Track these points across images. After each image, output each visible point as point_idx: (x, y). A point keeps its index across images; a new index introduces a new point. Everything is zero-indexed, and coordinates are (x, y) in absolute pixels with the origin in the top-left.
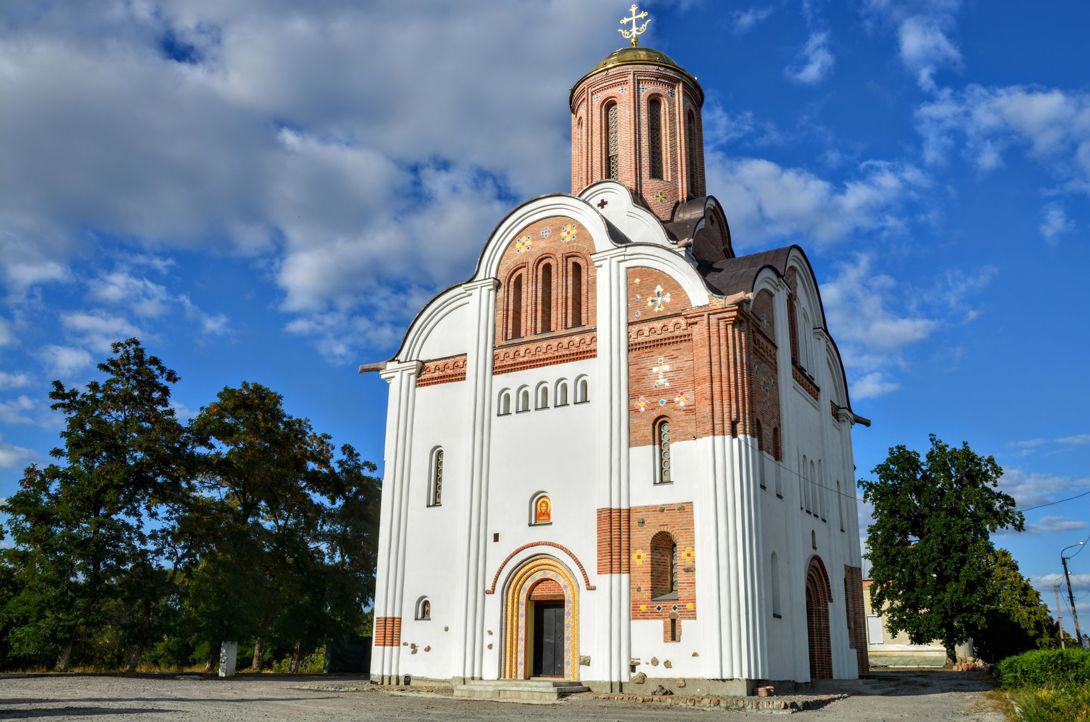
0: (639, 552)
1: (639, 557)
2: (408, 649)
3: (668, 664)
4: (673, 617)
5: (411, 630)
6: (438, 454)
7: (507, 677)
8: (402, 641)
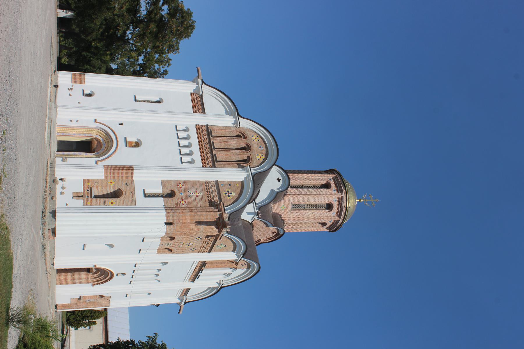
1: (111, 183)
3: (62, 193)
4: (84, 196)
5: (78, 88)
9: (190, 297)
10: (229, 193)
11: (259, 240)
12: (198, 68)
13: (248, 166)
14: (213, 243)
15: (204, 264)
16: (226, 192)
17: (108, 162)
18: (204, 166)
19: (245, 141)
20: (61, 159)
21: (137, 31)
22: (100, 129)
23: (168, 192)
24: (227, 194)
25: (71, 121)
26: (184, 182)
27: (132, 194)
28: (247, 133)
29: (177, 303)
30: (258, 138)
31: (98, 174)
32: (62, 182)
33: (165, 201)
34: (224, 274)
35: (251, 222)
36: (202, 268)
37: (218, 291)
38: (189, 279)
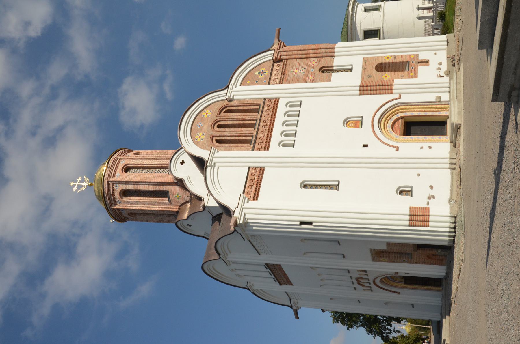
0: (384, 77)
1: (386, 77)
2: (432, 201)
3: (440, 64)
6: (245, 240)
7: (448, 106)
8: (427, 206)
17: (383, 98)
25: (430, 148)
27: (366, 67)
33: (332, 62)
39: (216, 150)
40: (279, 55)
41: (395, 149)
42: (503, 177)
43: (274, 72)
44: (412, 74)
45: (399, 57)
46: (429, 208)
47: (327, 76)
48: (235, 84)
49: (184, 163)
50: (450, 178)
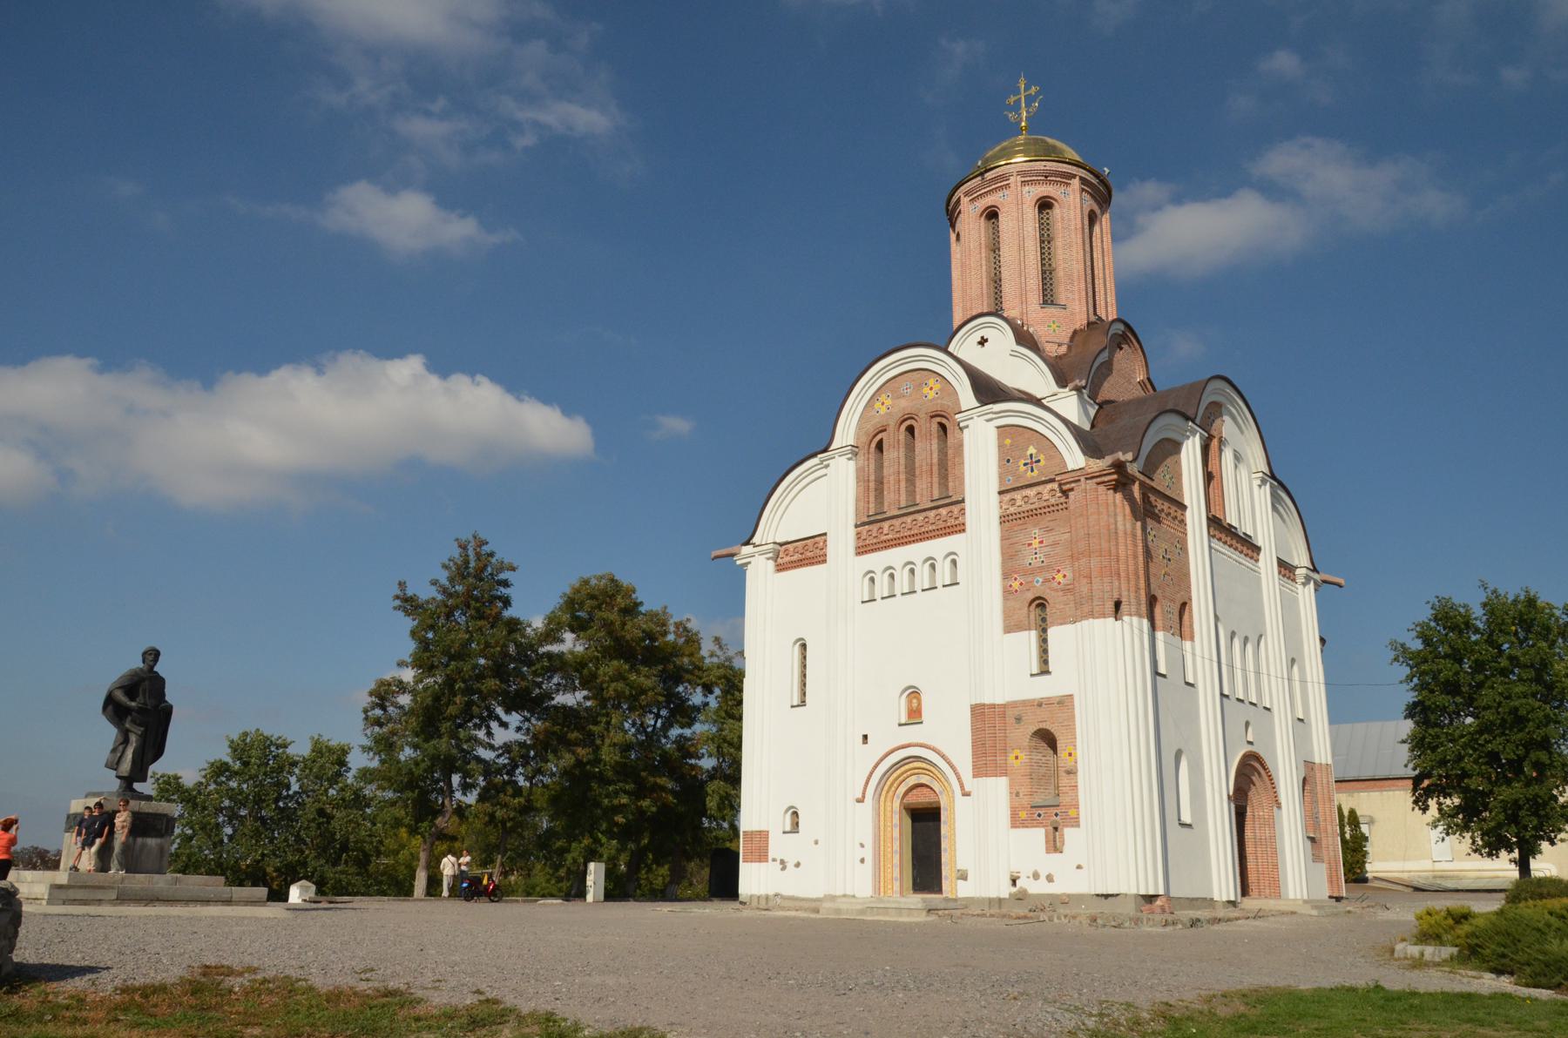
1: (1017, 758)
2: (778, 865)
3: (1050, 879)
5: (779, 845)
9: (1300, 558)
10: (1029, 461)
11: (1141, 383)
12: (713, 556)
13: (957, 416)
14: (1160, 499)
15: (1217, 524)
16: (1026, 471)
17: (965, 762)
18: (960, 528)
19: (891, 429)
20: (960, 882)
21: (553, 775)
22: (877, 796)
23: (1035, 613)
24: (1032, 467)
25: (862, 861)
26: (1006, 575)
27: (1044, 706)
28: (870, 427)
29: (1316, 590)
30: (883, 398)
31: (996, 791)
32: (1021, 878)
33: (1059, 621)
34: (1236, 467)
35: (1097, 407)
36: (1224, 527)
37: (1281, 484)
38: (1253, 561)
39: (850, 456)
40: (1073, 485)
41: (860, 796)
42: (844, 994)
43: (1031, 492)
44: (1023, 815)
45: (1073, 781)
46: (767, 861)
47: (1021, 621)
48: (994, 416)
49: (986, 341)
50: (811, 896)
